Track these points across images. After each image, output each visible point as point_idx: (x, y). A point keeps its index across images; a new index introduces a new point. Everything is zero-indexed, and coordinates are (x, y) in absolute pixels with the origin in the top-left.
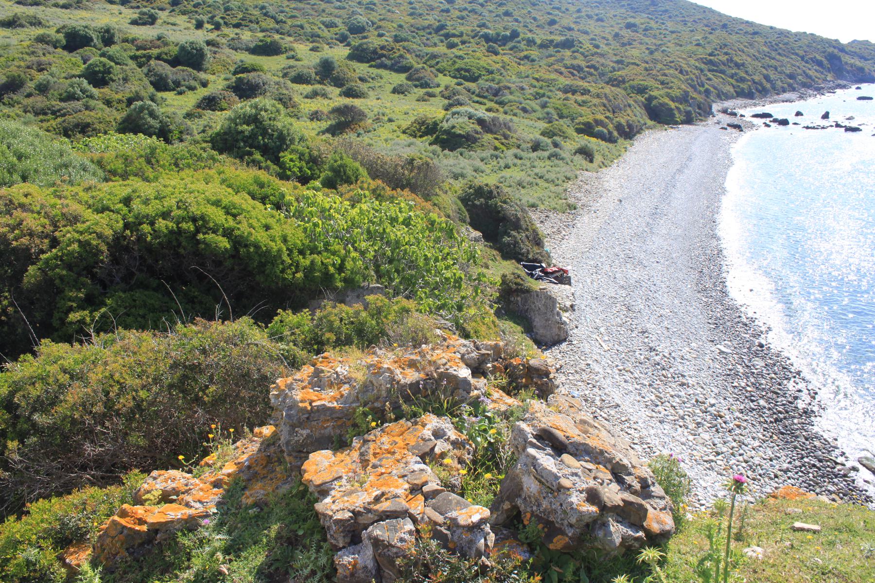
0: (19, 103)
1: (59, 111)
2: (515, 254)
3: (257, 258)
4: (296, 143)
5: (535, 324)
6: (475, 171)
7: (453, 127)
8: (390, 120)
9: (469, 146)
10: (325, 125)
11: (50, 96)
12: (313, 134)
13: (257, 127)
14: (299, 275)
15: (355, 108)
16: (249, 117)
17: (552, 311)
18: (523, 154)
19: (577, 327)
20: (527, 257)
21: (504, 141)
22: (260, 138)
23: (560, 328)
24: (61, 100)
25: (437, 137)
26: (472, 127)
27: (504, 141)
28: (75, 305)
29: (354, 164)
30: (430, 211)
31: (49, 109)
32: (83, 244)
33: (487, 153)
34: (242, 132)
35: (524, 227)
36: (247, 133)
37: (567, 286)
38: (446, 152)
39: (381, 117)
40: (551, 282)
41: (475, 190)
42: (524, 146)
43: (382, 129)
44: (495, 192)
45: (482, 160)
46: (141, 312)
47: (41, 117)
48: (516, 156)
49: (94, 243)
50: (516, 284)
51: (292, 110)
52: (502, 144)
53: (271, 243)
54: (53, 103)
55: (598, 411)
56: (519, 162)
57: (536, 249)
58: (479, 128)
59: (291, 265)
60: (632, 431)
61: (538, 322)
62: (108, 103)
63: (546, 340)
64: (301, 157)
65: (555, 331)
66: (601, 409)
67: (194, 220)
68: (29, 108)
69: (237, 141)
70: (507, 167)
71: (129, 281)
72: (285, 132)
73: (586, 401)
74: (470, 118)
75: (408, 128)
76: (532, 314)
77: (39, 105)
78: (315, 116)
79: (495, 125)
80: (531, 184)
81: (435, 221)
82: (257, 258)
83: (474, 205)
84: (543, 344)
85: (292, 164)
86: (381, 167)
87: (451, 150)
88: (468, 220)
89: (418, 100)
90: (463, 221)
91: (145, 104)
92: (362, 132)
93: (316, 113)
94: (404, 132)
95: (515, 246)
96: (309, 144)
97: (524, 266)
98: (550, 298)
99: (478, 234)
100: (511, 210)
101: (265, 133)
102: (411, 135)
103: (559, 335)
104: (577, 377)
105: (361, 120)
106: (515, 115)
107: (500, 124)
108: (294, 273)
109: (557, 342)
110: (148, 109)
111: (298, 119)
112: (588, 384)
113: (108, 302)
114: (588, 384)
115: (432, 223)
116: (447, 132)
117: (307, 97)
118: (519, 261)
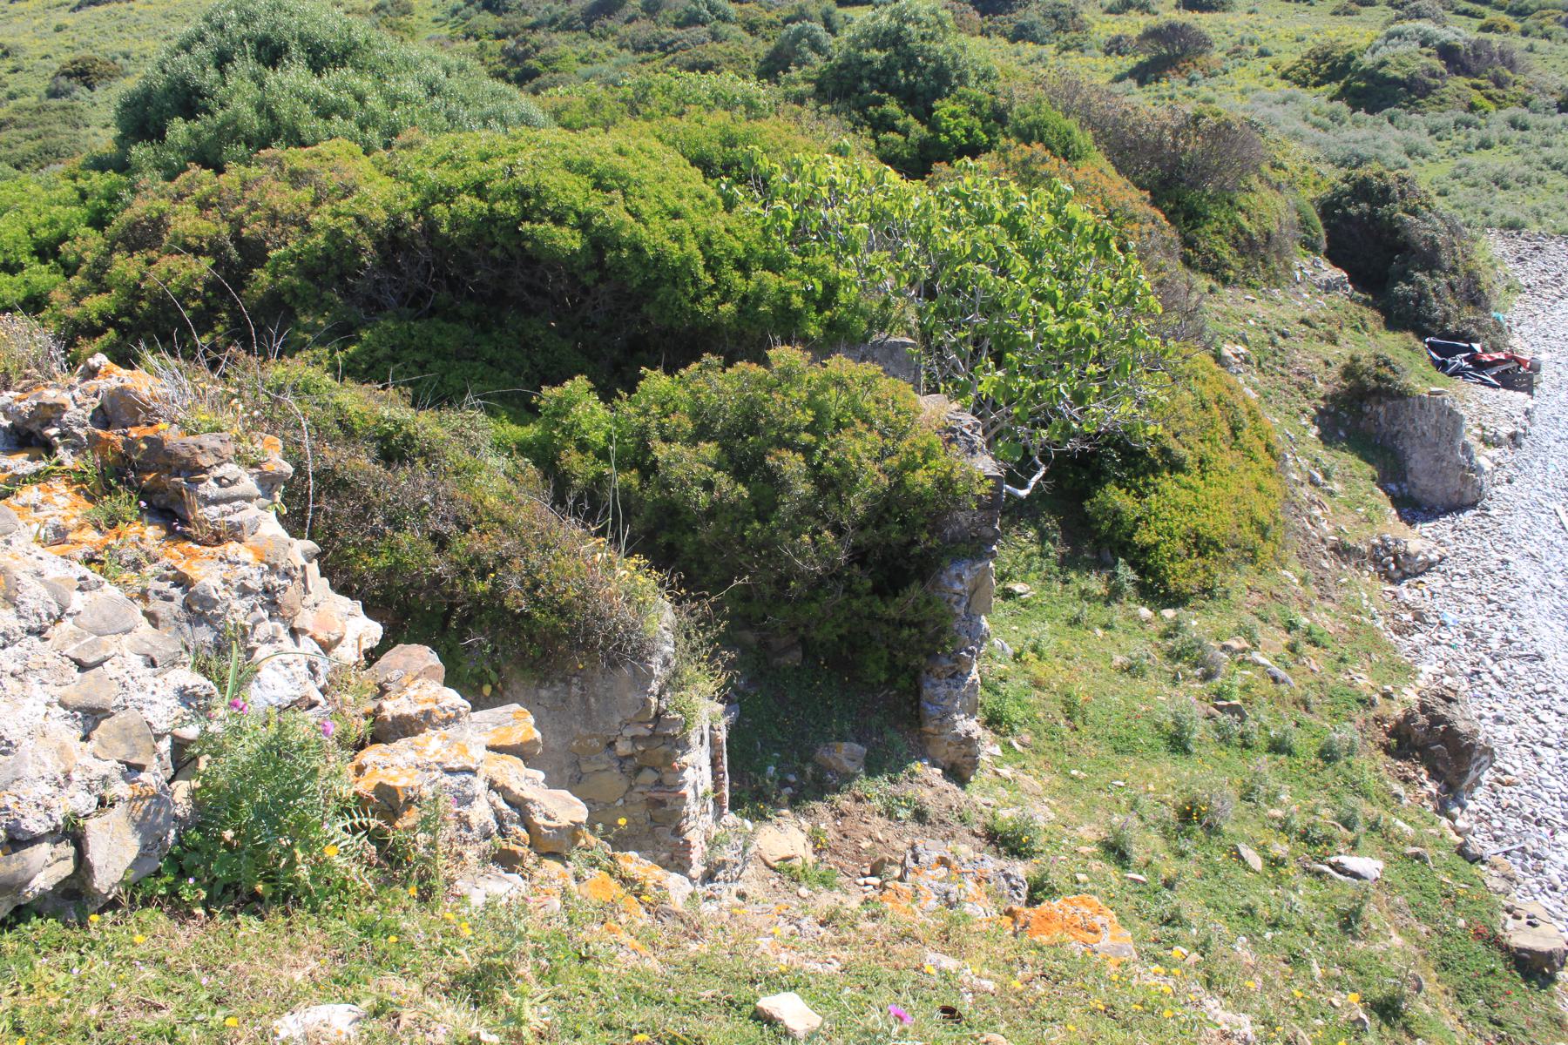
0: (614, 33)
1: (671, 44)
2: (1416, 319)
3: (635, 269)
4: (972, 83)
5: (1411, 464)
6: (1409, 154)
7: (1383, 64)
8: (1263, 54)
9: (1411, 102)
10: (1129, 62)
11: (660, 19)
12: (1102, 80)
13: (898, 54)
14: (727, 308)
15: (1190, 28)
16: (885, 34)
17: (1451, 441)
18: (1531, 118)
19: (1509, 481)
20: (1442, 327)
21: (1493, 91)
22: (901, 73)
23: (1465, 479)
24: (678, 26)
25: (1347, 85)
26: (1422, 62)
27: (1493, 91)
28: (310, 338)
29: (1065, 122)
30: (1068, 197)
31: (656, 41)
32: (335, 234)
33: (1446, 118)
34: (870, 62)
35: (1447, 264)
36: (877, 65)
37: (1522, 396)
38: (1361, 114)
39: (1246, 46)
40: (1484, 383)
41: (1355, 186)
42: (1538, 101)
43: (1241, 70)
44: (1395, 191)
45: (1431, 132)
46: (419, 357)
47: (644, 55)
48: (1513, 124)
49: (349, 232)
50: (1377, 377)
51: (1074, 34)
52: (1489, 97)
53: (668, 244)
54: (664, 30)
55: (1488, 661)
56: (1518, 134)
57: (1467, 313)
58: (1438, 65)
59: (714, 287)
60: (1550, 718)
61: (1418, 461)
62: (752, 28)
63: (1433, 500)
64: (976, 108)
65: (1454, 483)
66: (1495, 658)
67: (523, 195)
68: (628, 41)
69: (860, 79)
70: (1485, 145)
71: (416, 303)
72: (948, 62)
73: (1469, 636)
74: (1423, 44)
75: (1294, 69)
76: (1407, 443)
77: (644, 35)
78: (1115, 47)
79: (1477, 57)
80: (1525, 181)
81: (1073, 221)
82: (635, 269)
83: (1347, 217)
84: (1413, 508)
85: (952, 122)
86: (1132, 129)
87: (1370, 111)
88: (1324, 245)
89: (1335, 13)
90: (1310, 246)
91: (804, 28)
92: (1199, 75)
93: (1118, 39)
94: (1284, 77)
95: (1418, 304)
96: (998, 86)
97: (1432, 346)
98: (1451, 412)
99: (1338, 274)
100: (1420, 229)
101: (910, 63)
102: (1297, 82)
103: (1462, 494)
104: (1472, 584)
105: (1201, 52)
106: (1547, 36)
107: (1491, 56)
108: (717, 303)
109: (1457, 506)
110: (808, 36)
111: (1082, 51)
112: (1490, 602)
113: (365, 335)
114: (1490, 602)
115: (1069, 225)
116: (1369, 75)
117: (1110, 11)
118: (1421, 335)
